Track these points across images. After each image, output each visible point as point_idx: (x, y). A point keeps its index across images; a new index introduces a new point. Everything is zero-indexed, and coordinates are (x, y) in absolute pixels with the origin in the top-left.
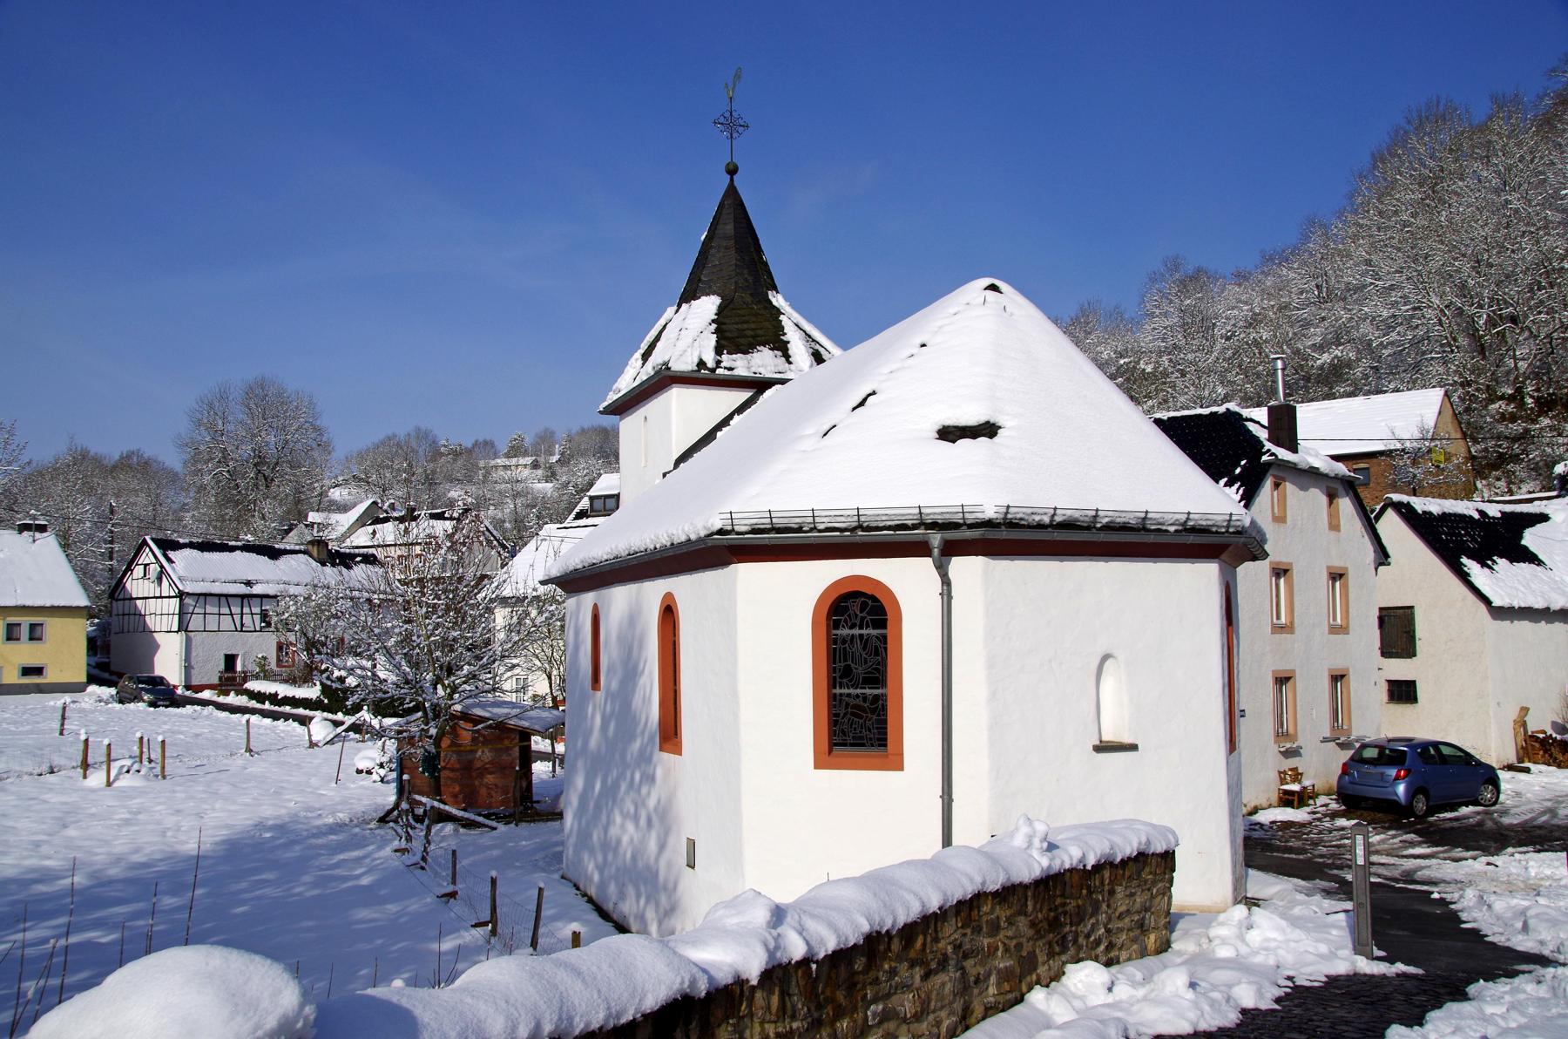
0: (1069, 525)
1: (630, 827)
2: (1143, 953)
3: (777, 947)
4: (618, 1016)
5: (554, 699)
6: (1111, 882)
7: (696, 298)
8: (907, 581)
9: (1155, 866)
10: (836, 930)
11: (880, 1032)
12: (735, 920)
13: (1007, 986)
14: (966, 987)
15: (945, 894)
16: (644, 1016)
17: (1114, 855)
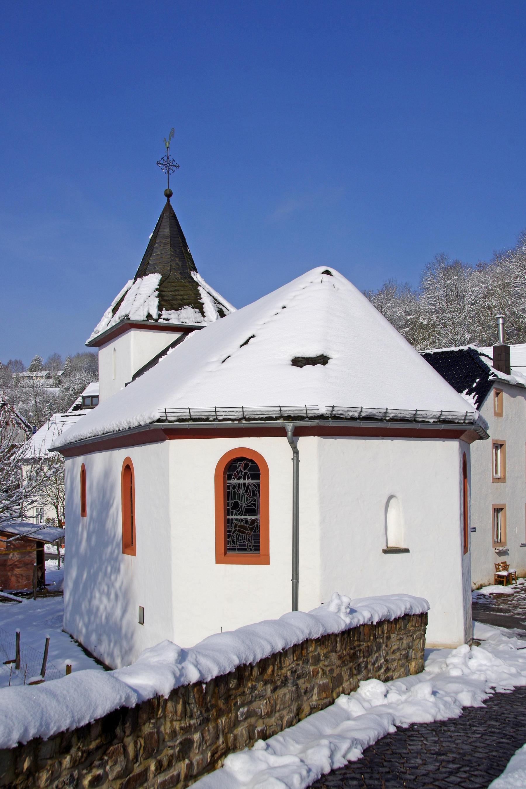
0: (369, 418)
1: (105, 600)
2: (408, 673)
3: (181, 675)
4: (79, 721)
5: (60, 521)
6: (388, 632)
7: (146, 275)
8: (272, 451)
9: (415, 621)
10: (218, 664)
11: (246, 724)
12: (156, 659)
13: (324, 695)
14: (298, 697)
15: (286, 641)
16: (97, 721)
17: (390, 615)
